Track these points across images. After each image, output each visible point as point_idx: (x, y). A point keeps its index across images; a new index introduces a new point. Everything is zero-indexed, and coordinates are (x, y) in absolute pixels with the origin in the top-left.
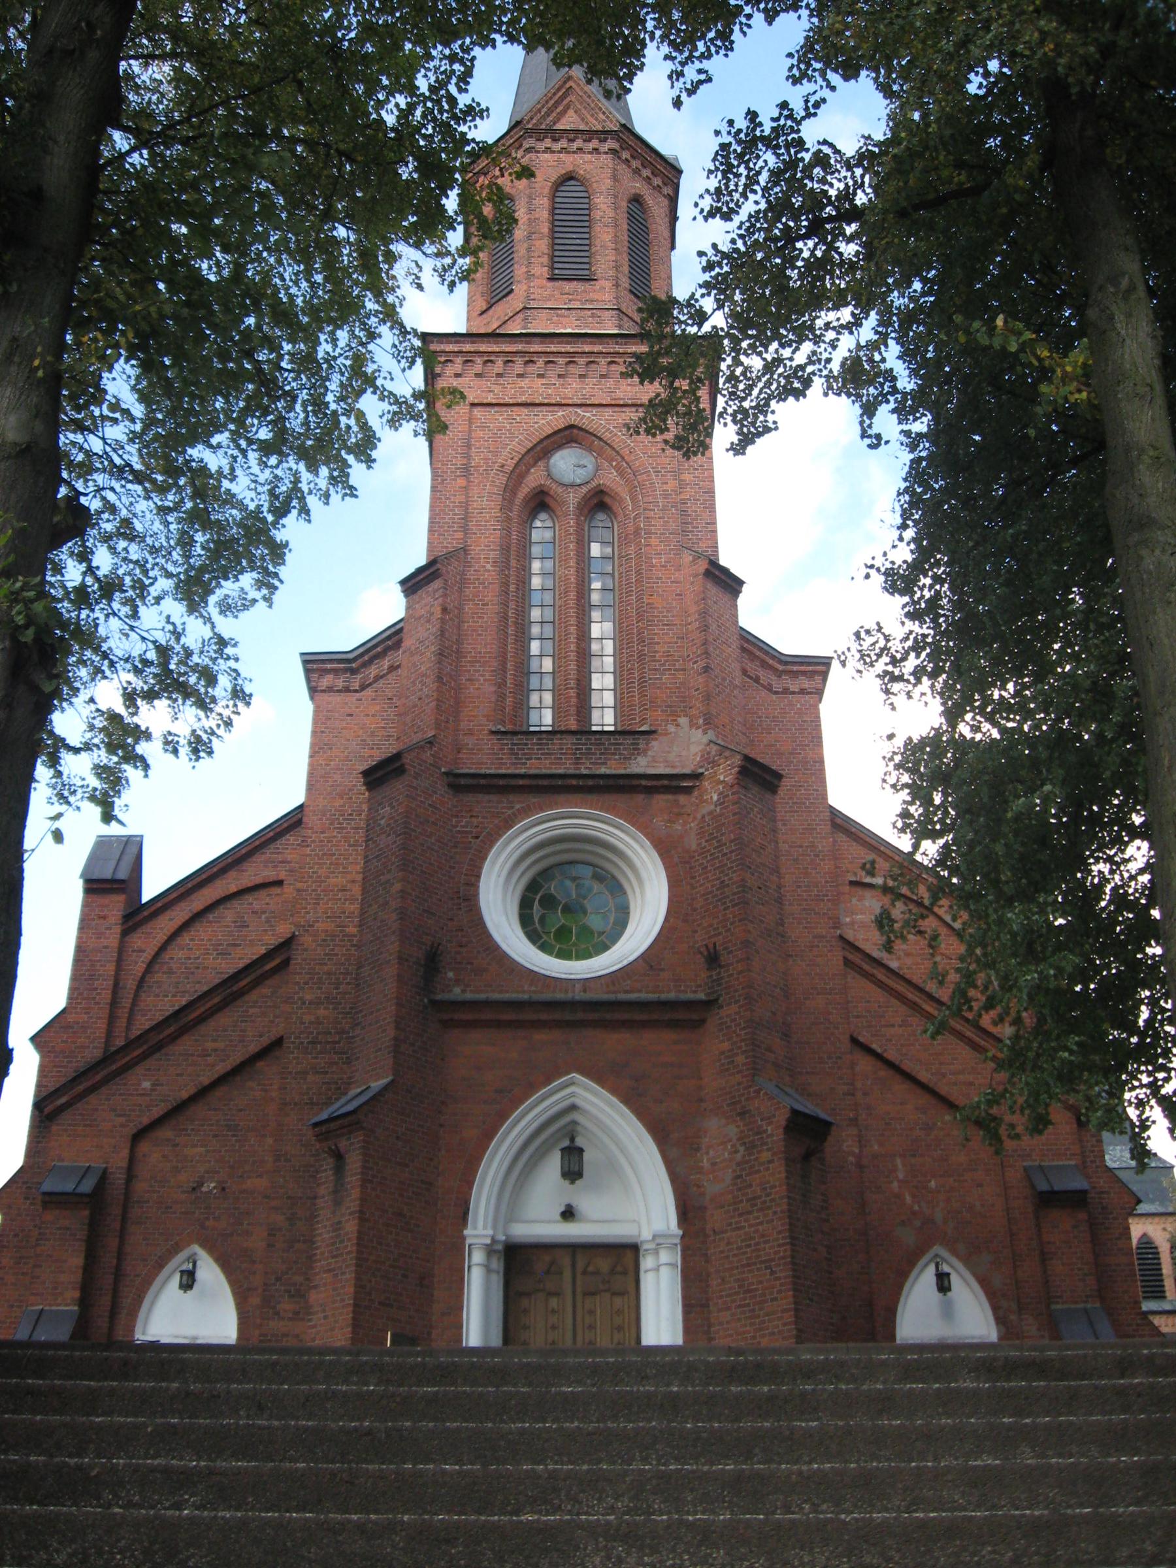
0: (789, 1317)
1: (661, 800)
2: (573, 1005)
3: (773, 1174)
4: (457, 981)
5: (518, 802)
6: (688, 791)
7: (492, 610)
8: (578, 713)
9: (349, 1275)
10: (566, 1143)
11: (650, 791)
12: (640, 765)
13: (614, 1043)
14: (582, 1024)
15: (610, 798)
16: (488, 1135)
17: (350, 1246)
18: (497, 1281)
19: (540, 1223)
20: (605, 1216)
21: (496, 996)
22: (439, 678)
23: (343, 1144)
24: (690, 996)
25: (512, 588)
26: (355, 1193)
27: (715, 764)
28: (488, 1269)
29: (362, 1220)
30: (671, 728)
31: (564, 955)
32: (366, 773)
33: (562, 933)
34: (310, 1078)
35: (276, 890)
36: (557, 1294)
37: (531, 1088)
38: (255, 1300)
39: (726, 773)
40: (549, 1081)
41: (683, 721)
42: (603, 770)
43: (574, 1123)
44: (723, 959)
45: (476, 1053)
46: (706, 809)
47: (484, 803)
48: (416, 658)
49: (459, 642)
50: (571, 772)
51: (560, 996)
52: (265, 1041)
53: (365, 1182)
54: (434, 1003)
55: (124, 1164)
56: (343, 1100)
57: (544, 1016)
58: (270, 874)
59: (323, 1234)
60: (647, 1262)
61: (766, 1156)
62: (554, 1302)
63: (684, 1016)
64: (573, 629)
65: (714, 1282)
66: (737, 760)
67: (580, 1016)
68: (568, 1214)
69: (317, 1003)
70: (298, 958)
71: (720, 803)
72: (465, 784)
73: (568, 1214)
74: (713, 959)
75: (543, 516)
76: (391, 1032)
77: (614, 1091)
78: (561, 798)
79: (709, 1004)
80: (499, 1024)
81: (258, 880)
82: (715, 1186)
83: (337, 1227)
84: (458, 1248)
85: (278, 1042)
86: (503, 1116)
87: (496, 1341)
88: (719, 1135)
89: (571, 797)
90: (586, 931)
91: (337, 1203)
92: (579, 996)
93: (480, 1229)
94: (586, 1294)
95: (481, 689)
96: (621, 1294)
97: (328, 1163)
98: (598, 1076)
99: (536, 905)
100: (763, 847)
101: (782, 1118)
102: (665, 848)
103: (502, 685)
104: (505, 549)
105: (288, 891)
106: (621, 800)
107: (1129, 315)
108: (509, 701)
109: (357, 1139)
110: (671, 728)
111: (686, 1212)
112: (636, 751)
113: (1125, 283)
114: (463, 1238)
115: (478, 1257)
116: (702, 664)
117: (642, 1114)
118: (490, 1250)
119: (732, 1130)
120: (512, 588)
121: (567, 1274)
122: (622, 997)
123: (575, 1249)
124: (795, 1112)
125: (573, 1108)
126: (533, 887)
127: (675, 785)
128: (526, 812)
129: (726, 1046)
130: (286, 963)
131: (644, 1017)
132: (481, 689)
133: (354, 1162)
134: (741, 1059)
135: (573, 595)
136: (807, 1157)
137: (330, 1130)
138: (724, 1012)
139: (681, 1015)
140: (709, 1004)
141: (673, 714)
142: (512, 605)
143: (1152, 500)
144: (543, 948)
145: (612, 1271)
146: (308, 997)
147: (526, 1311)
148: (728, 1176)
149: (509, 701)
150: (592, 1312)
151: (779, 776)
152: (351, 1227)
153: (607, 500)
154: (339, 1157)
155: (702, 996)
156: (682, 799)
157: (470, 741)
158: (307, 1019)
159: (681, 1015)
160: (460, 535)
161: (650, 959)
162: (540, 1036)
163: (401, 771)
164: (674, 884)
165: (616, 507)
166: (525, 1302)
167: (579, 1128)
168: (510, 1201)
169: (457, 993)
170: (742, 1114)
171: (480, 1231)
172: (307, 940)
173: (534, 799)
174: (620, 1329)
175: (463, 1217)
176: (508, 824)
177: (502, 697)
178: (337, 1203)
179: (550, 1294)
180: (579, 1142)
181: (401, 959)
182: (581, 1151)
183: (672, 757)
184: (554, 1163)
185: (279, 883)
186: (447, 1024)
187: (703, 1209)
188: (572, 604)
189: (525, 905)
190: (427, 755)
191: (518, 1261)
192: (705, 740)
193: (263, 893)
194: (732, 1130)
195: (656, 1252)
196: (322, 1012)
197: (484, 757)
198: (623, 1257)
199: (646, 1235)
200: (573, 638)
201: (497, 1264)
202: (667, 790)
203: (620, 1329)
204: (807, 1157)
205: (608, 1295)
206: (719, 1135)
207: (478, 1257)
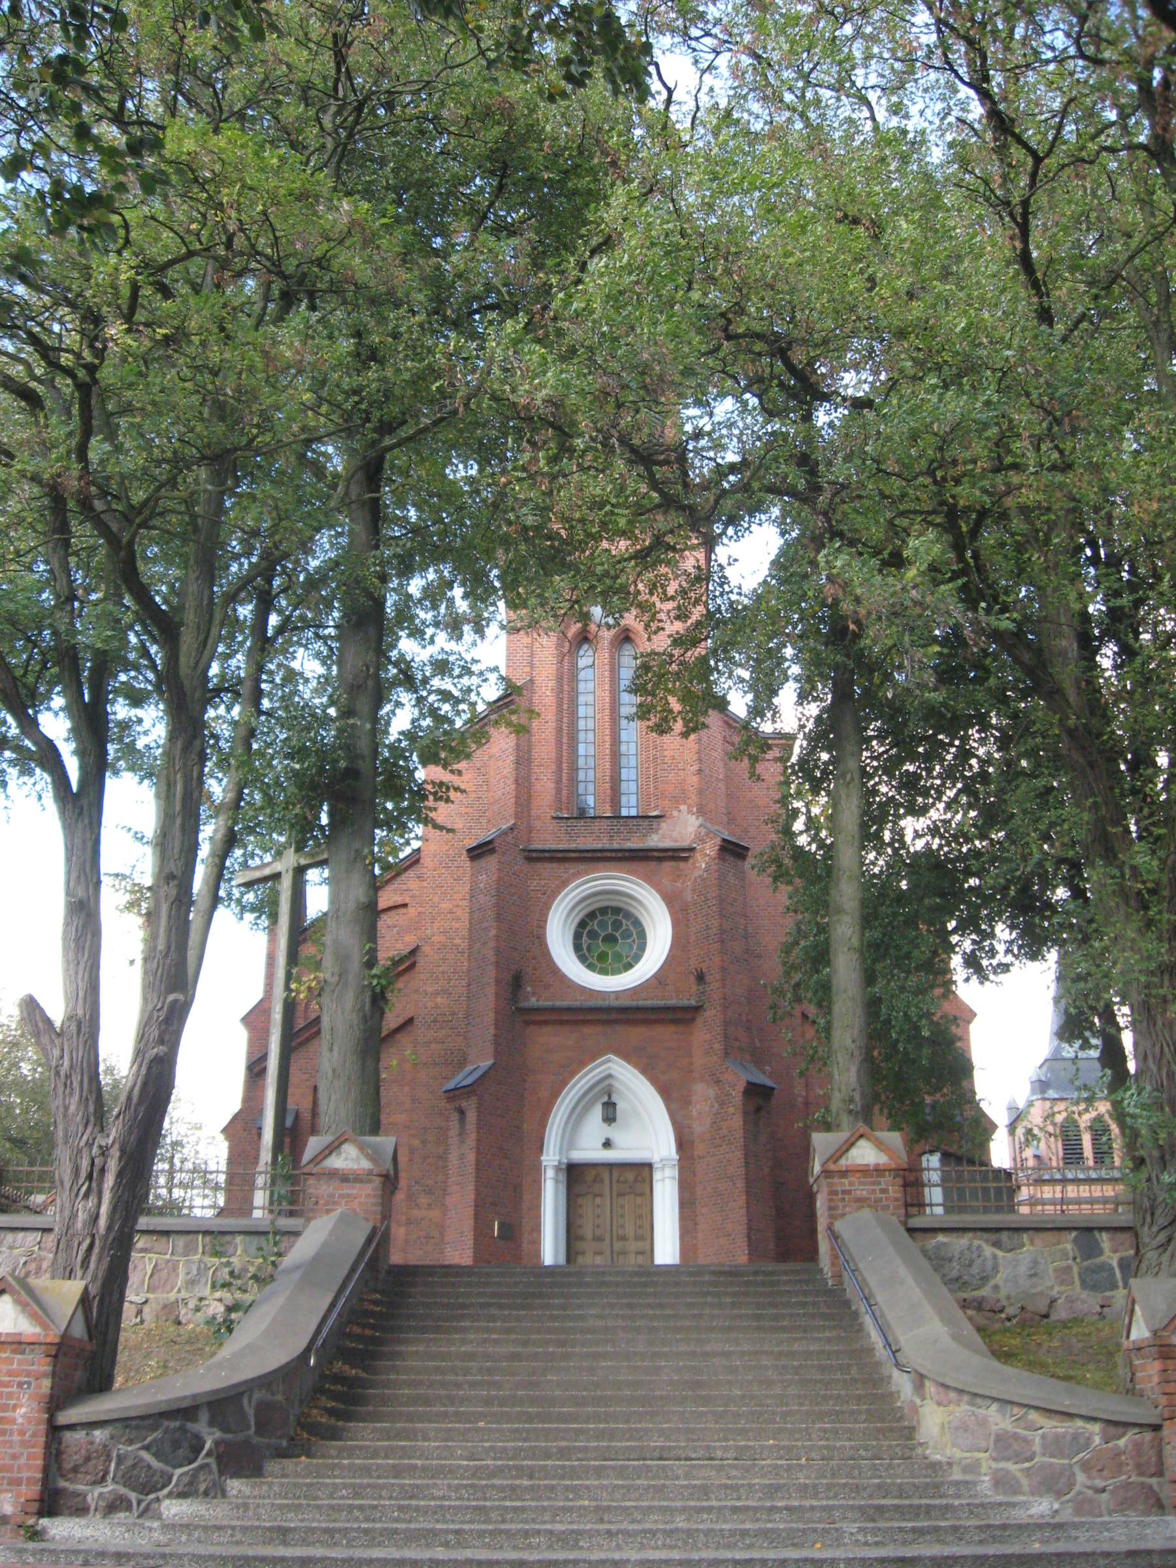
0: (743, 1212)
1: (668, 866)
2: (608, 1010)
3: (735, 1122)
4: (534, 994)
5: (572, 868)
6: (686, 859)
7: (552, 725)
8: (612, 801)
9: (471, 1187)
10: (605, 1099)
11: (660, 859)
12: (655, 841)
13: (636, 1034)
14: (616, 1022)
15: (634, 865)
16: (555, 1095)
17: (471, 1169)
18: (563, 1188)
19: (589, 1150)
20: (628, 1148)
21: (559, 1003)
22: (516, 781)
23: (464, 1104)
24: (685, 1002)
25: (565, 707)
26: (473, 1136)
27: (703, 841)
28: (556, 1181)
29: (478, 1153)
30: (675, 813)
31: (603, 972)
32: (469, 851)
33: (602, 957)
34: (433, 1046)
35: (403, 910)
36: (600, 1195)
37: (582, 1064)
38: (174, 1028)
39: (710, 849)
40: (594, 1060)
41: (683, 808)
42: (629, 845)
43: (610, 1085)
44: (708, 978)
45: (547, 1041)
46: (697, 873)
47: (547, 869)
48: (500, 763)
49: (529, 752)
50: (607, 846)
51: (600, 1003)
52: (401, 1021)
53: (479, 1128)
54: (519, 1010)
55: (310, 1106)
56: (461, 1075)
57: (589, 1017)
58: (398, 899)
59: (453, 1160)
60: (657, 1176)
61: (732, 1110)
62: (598, 1200)
63: (684, 1016)
64: (607, 738)
65: (699, 1190)
66: (718, 841)
67: (613, 1016)
68: (607, 1144)
69: (436, 993)
70: (421, 962)
71: (706, 870)
72: (535, 857)
73: (607, 1144)
74: (701, 978)
75: (585, 647)
76: (492, 1031)
77: (636, 1066)
78: (600, 865)
79: (697, 1009)
80: (562, 1023)
81: (391, 904)
82: (700, 1128)
83: (462, 1157)
84: (537, 1169)
85: (410, 1021)
86: (564, 1083)
87: (562, 1260)
88: (703, 1095)
89: (607, 864)
90: (618, 957)
91: (462, 1142)
92: (615, 1003)
93: (551, 1158)
94: (619, 1195)
95: (545, 785)
96: (641, 1195)
97: (455, 1116)
98: (627, 1057)
99: (585, 937)
100: (735, 900)
101: (741, 1086)
102: (670, 900)
103: (559, 781)
104: (560, 679)
105: (412, 911)
106: (641, 867)
107: (848, 796)
108: (565, 793)
109: (473, 1101)
110: (675, 813)
111: (683, 1144)
112: (651, 830)
113: (849, 777)
114: (540, 1162)
115: (550, 1173)
116: (696, 767)
117: (654, 1081)
118: (557, 1169)
119: (711, 1092)
120: (565, 707)
121: (607, 1182)
122: (641, 1003)
123: (611, 1166)
124: (749, 1083)
125: (610, 1076)
126: (582, 924)
127: (677, 855)
128: (579, 874)
129: (707, 1037)
130: (413, 965)
131: (654, 1017)
132: (545, 785)
133: (472, 1116)
134: (717, 1046)
135: (607, 712)
136: (758, 1110)
137: (453, 1095)
138: (708, 1014)
139: (680, 1016)
140: (697, 1009)
141: (677, 801)
142: (565, 720)
143: (844, 899)
144: (590, 967)
145: (636, 1181)
146: (430, 990)
147: (580, 1206)
148: (708, 1121)
149: (565, 793)
150: (622, 1207)
151: (747, 849)
152: (471, 1157)
153: (632, 635)
154: (462, 1112)
155: (693, 1003)
156: (682, 865)
157: (538, 824)
158: (430, 1005)
159: (680, 1016)
160: (528, 669)
161: (659, 978)
162: (587, 1030)
163: (492, 851)
164: (676, 924)
165: (637, 641)
166: (580, 1200)
167: (616, 1084)
168: (571, 1135)
169: (533, 1002)
170: (718, 1082)
171: (551, 1157)
172: (426, 949)
173: (582, 867)
174: (640, 1216)
175: (540, 1149)
176: (565, 884)
177: (559, 790)
178: (462, 1142)
179: (596, 1195)
180: (614, 1099)
181: (498, 982)
182: (615, 1104)
183: (675, 834)
184: (597, 1112)
185: (405, 905)
186: (527, 1023)
187: (693, 1142)
188: (607, 719)
189: (577, 936)
190: (510, 838)
191: (576, 1175)
192: (698, 823)
193: (393, 913)
194: (711, 1092)
195: (663, 1169)
196: (439, 1000)
197: (549, 837)
198: (642, 1171)
199: (656, 1159)
200: (608, 745)
201: (563, 1177)
202: (673, 858)
203: (640, 1216)
204: (758, 1110)
205: (631, 1197)
206: (703, 1095)
207: (550, 1173)
